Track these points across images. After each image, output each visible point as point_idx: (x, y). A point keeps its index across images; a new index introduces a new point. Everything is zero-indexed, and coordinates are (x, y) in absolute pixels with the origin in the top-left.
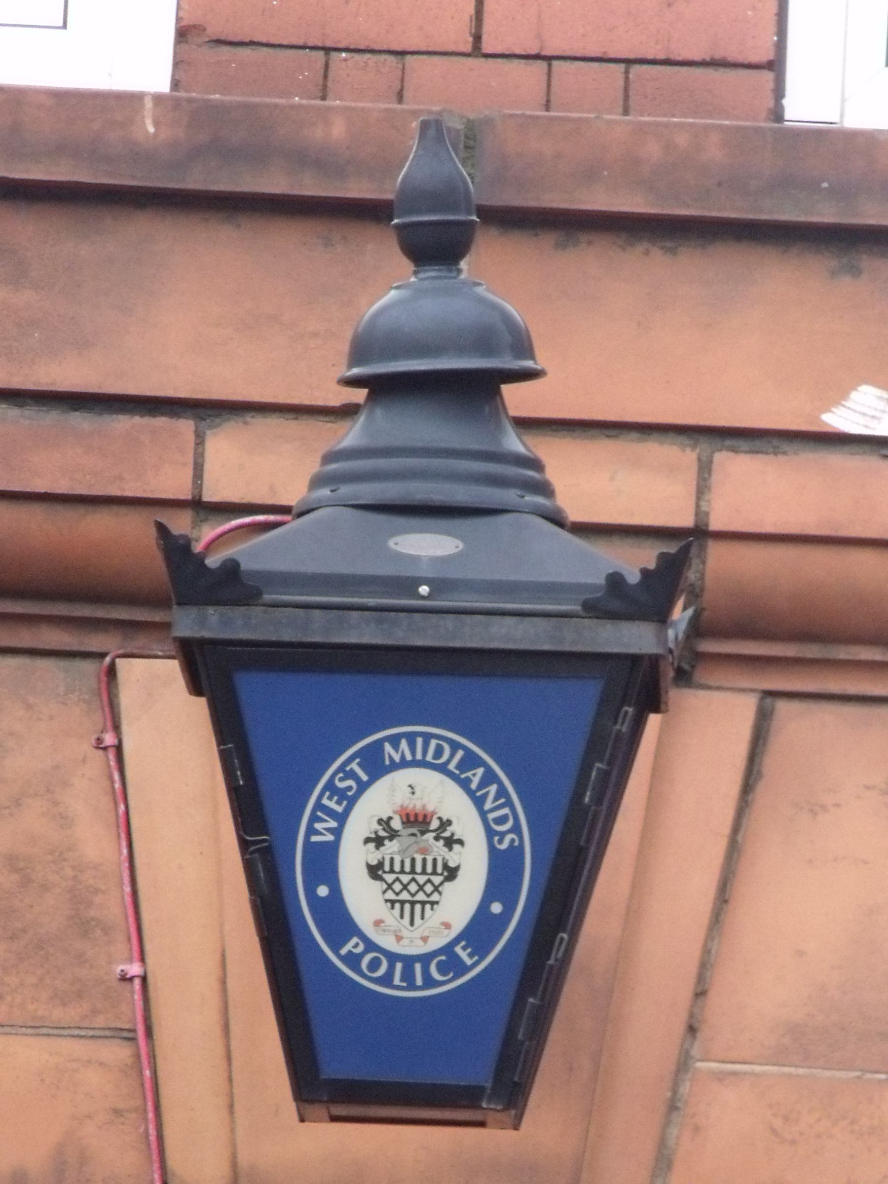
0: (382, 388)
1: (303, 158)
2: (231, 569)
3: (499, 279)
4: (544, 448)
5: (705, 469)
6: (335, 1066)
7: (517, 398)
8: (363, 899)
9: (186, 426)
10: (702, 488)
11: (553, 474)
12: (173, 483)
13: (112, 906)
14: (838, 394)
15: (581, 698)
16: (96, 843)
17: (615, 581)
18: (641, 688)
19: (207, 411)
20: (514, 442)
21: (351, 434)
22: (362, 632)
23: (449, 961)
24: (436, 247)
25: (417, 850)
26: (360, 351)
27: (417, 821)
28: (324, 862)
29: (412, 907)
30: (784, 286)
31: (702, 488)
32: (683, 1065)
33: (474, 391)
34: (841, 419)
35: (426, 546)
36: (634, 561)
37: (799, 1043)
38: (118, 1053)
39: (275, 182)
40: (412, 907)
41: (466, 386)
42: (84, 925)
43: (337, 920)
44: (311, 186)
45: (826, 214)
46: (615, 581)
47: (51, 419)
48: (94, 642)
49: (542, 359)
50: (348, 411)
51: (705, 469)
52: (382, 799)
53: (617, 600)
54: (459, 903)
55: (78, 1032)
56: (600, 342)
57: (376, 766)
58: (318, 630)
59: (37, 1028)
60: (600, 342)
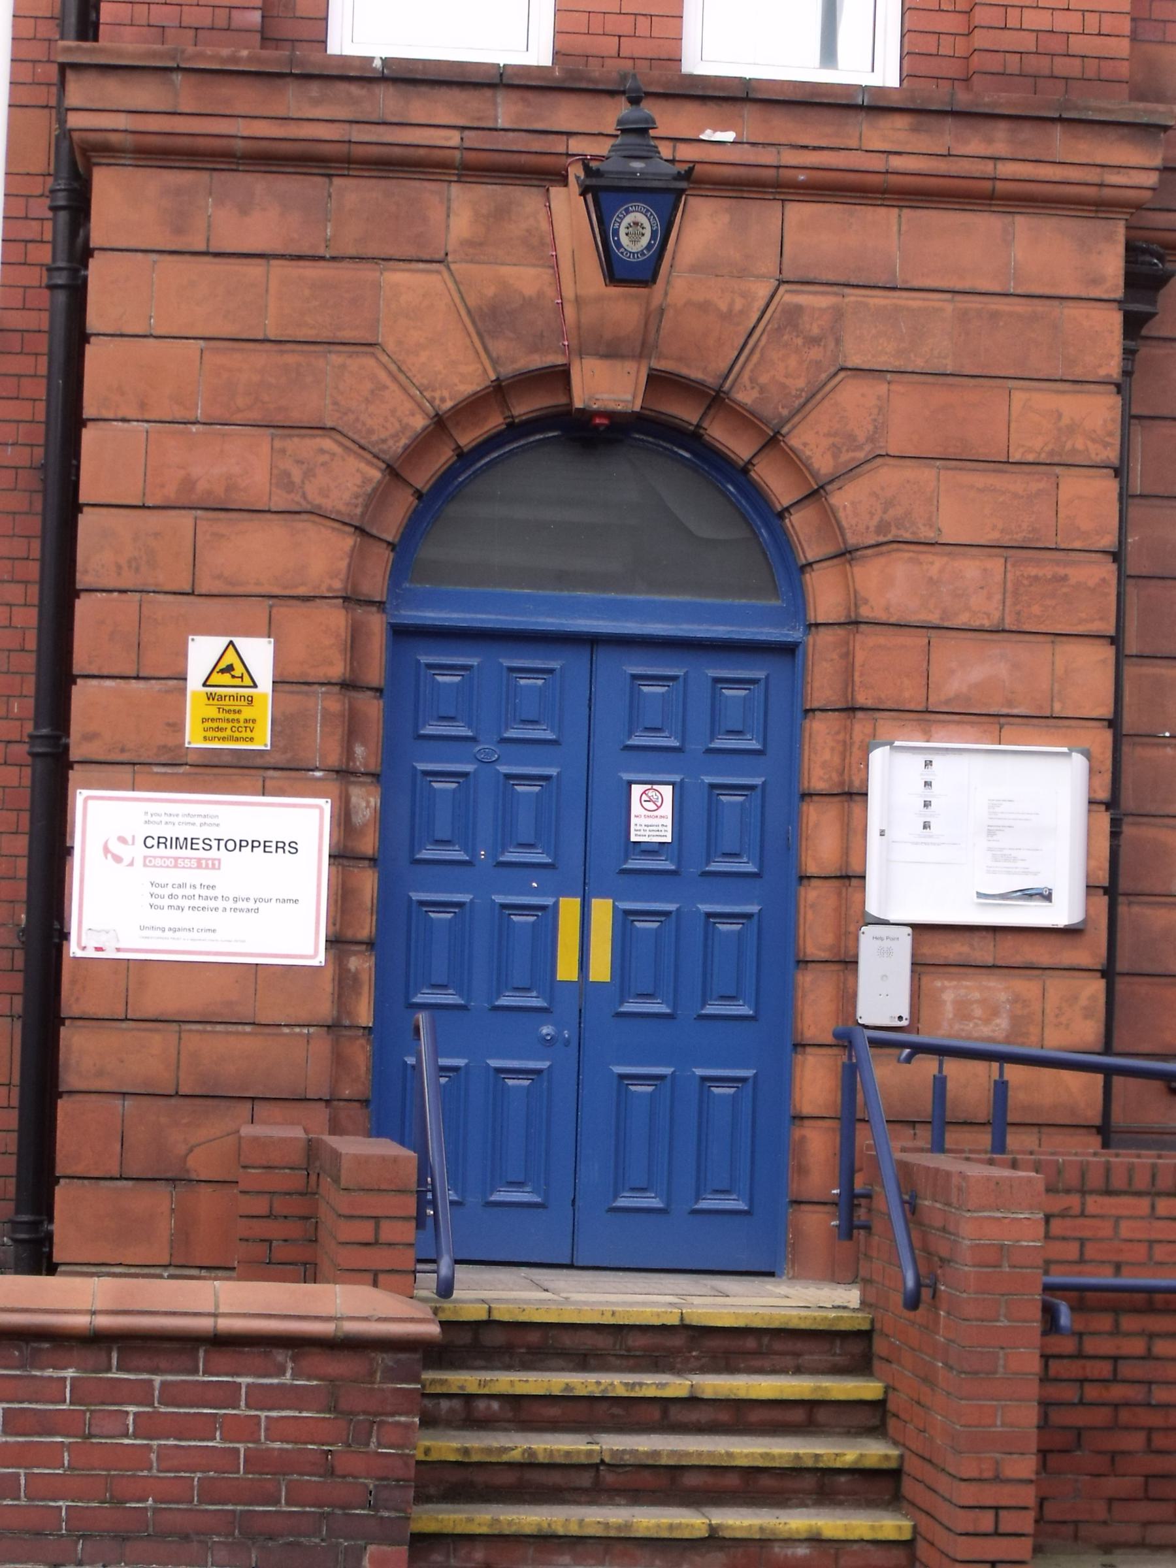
0: (623, 131)
1: (590, 80)
2: (598, 170)
3: (649, 108)
4: (657, 143)
5: (674, 147)
6: (618, 274)
7: (652, 133)
8: (624, 240)
9: (565, 138)
10: (674, 151)
11: (660, 149)
12: (562, 150)
13: (549, 239)
14: (702, 131)
15: (668, 196)
16: (545, 226)
17: (679, 173)
18: (680, 192)
19: (569, 134)
20: (652, 143)
21: (618, 141)
22: (625, 184)
23: (643, 254)
24: (635, 101)
25: (634, 230)
26: (620, 122)
27: (636, 224)
28: (616, 232)
29: (634, 242)
30: (690, 108)
31: (674, 151)
32: (670, 273)
33: (643, 132)
34: (702, 137)
35: (637, 165)
36: (683, 168)
37: (693, 269)
38: (551, 271)
39: (583, 85)
40: (634, 242)
41: (639, 131)
42: (543, 244)
43: (619, 244)
44: (591, 86)
45: (700, 93)
46: (679, 173)
47: (536, 136)
48: (544, 183)
49: (658, 124)
50: (616, 136)
51: (674, 147)
52: (629, 219)
53: (679, 177)
54: (645, 241)
55: (543, 266)
56: (669, 121)
57: (627, 212)
58: (616, 183)
59: (534, 266)
60: (669, 121)
